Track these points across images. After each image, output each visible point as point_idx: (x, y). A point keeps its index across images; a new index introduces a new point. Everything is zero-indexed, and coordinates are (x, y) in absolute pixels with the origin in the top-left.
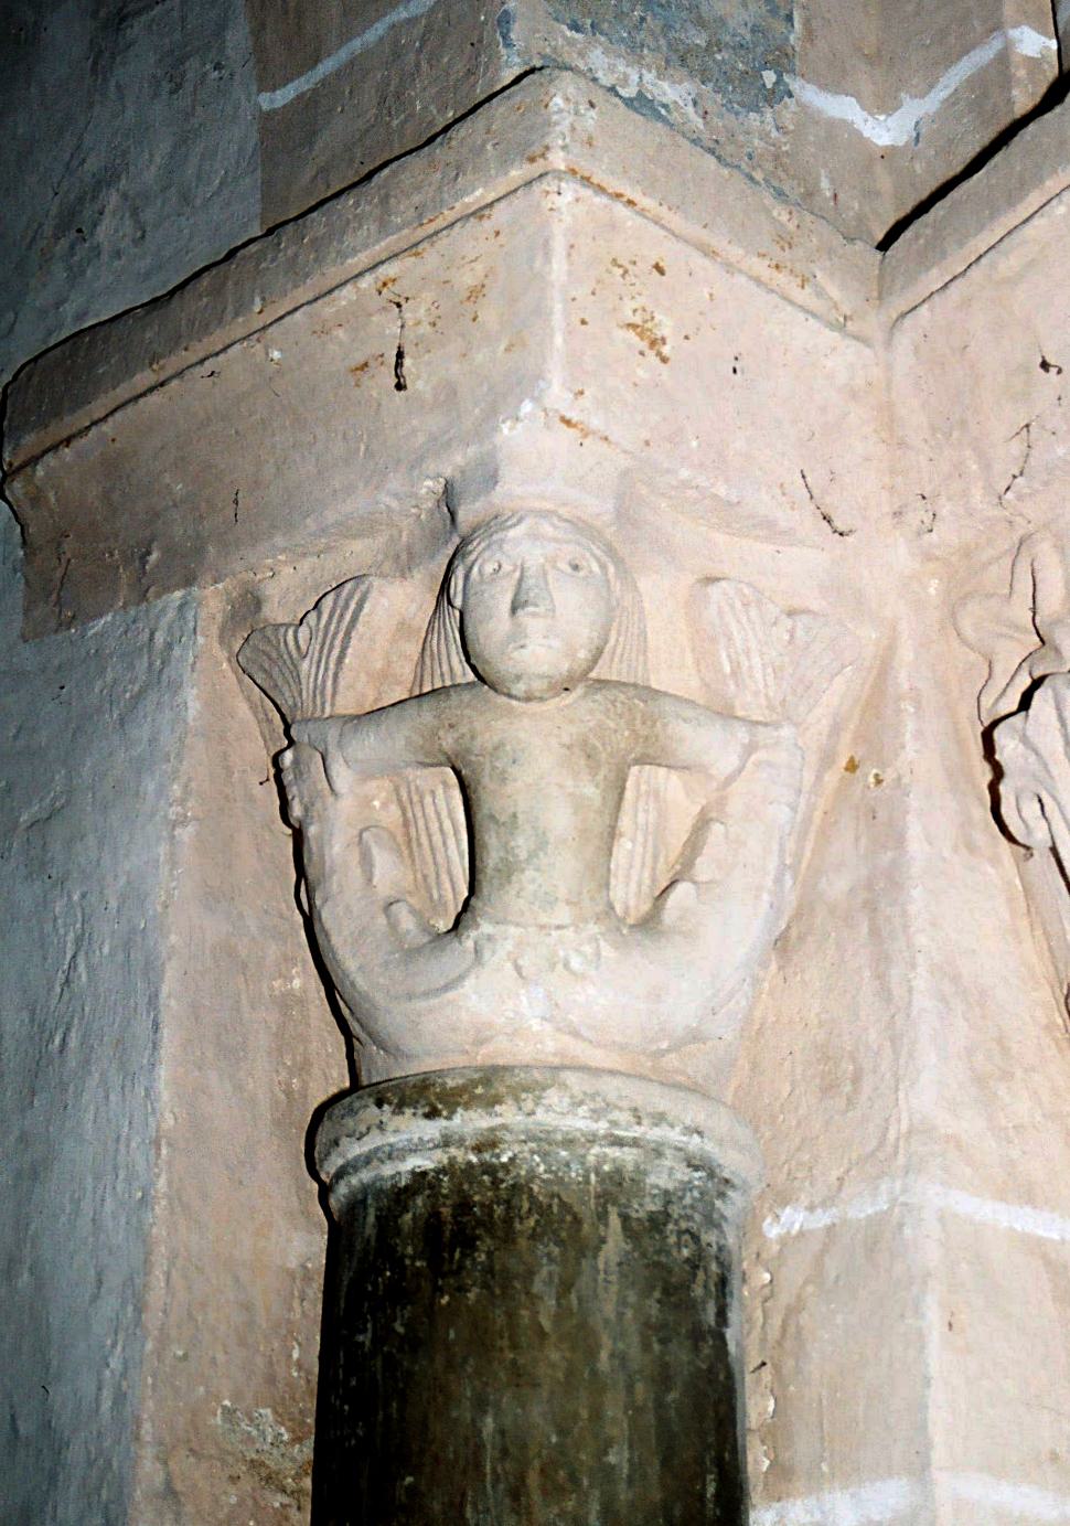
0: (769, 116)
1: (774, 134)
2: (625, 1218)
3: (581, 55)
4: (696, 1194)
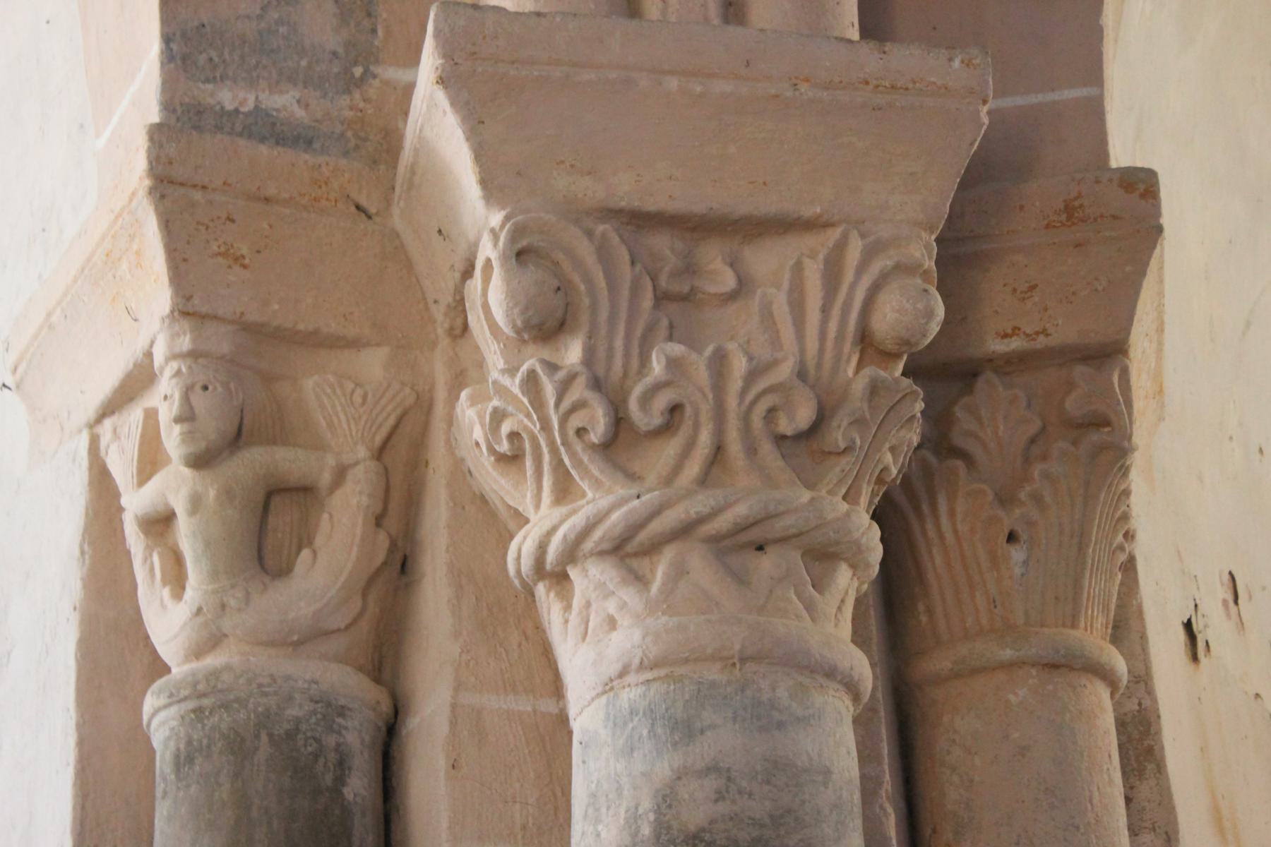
0: (357, 95)
1: (361, 105)
2: (270, 735)
3: (212, 95)
4: (319, 716)
